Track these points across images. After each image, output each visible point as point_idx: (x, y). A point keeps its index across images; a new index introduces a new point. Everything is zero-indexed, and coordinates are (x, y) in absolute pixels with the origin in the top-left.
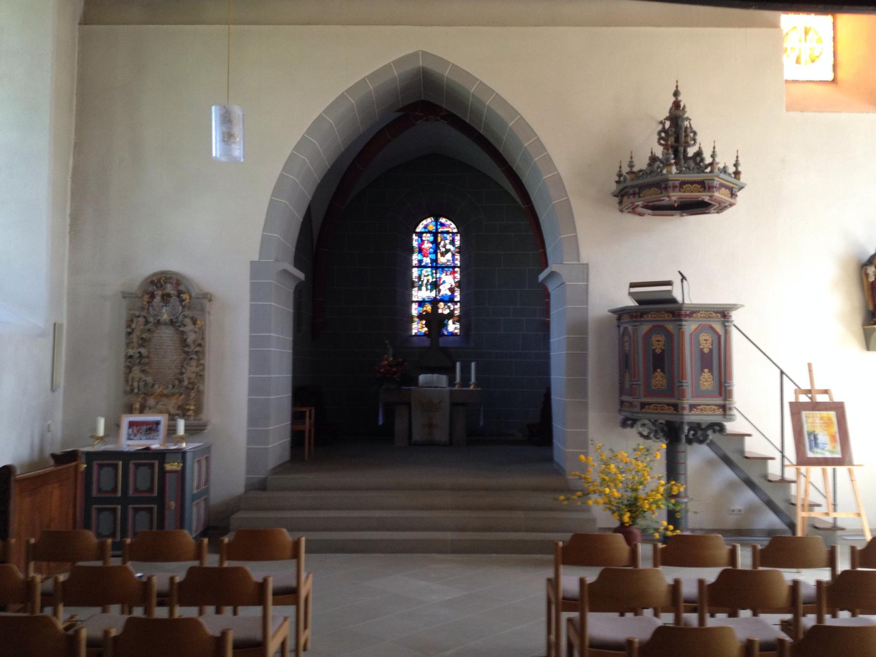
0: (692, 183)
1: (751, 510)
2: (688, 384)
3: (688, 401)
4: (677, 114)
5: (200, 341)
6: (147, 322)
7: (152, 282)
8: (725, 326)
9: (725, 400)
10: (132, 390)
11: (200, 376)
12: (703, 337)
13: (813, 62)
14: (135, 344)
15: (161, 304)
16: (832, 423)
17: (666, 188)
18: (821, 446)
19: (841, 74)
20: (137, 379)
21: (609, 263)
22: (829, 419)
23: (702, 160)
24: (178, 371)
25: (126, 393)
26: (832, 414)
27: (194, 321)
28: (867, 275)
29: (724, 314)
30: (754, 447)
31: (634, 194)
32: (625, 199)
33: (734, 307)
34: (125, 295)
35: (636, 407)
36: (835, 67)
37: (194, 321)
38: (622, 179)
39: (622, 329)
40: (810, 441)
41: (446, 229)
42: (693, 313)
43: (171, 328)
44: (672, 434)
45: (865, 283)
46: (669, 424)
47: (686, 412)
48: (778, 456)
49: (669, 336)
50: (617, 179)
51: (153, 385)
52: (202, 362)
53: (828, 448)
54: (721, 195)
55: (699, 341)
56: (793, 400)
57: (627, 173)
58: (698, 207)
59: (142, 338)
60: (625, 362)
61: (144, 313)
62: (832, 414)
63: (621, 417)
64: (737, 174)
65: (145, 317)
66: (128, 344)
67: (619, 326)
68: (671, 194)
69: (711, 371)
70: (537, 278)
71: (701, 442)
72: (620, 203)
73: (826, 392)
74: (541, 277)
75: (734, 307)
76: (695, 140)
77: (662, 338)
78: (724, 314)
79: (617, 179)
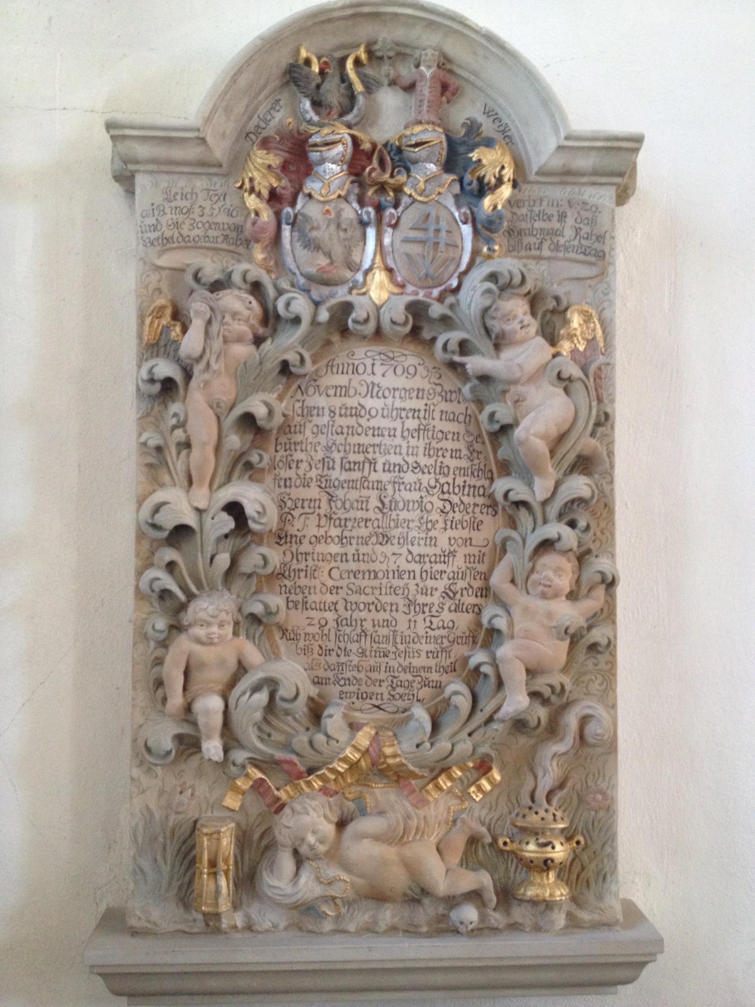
5: (588, 444)
6: (271, 320)
7: (294, 76)
10: (189, 744)
11: (590, 648)
14: (202, 456)
15: (350, 211)
20: (220, 676)
24: (464, 621)
25: (145, 753)
27: (550, 318)
34: (136, 155)
37: (550, 318)
41: (363, 566)
43: (410, 358)
51: (316, 712)
52: (602, 564)
59: (248, 420)
61: (254, 263)
65: (256, 288)
66: (155, 461)
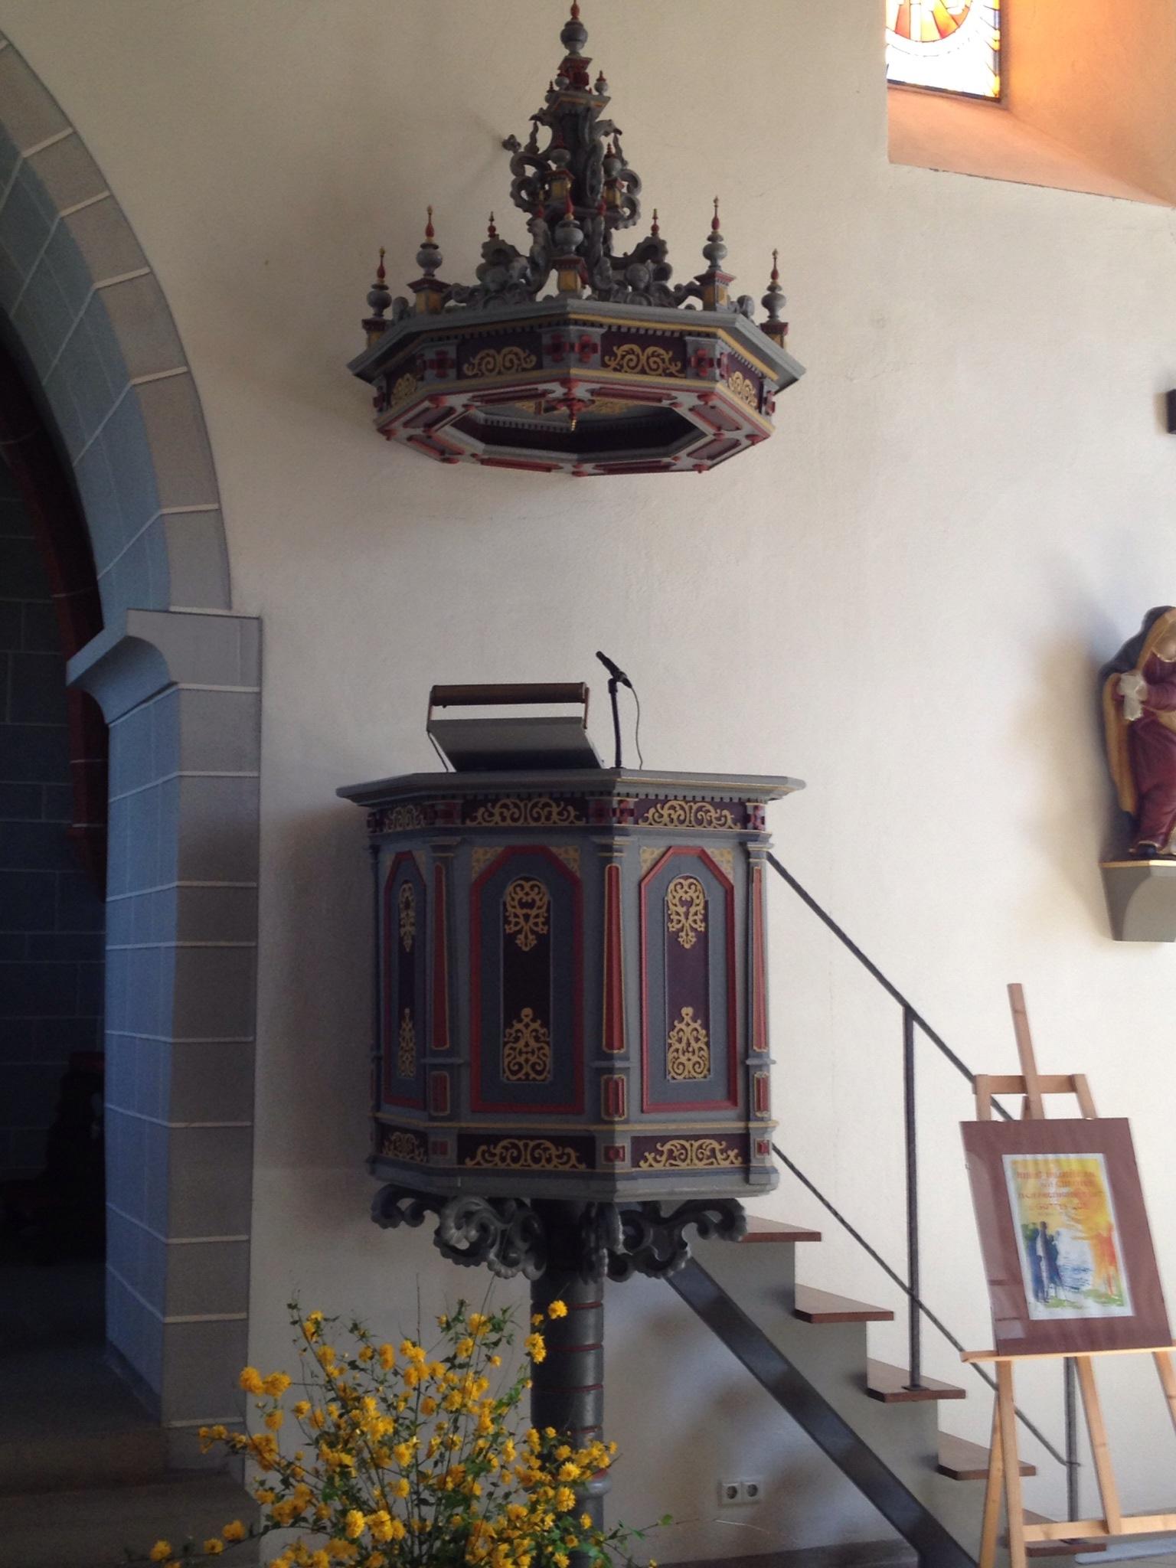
0: (644, 339)
1: (791, 1482)
2: (629, 1062)
3: (626, 1130)
4: (573, 106)
8: (747, 854)
9: (747, 1118)
12: (679, 891)
13: (943, 34)
16: (1098, 1193)
17: (558, 350)
18: (1067, 1277)
19: (1023, 81)
21: (342, 621)
22: (1089, 1180)
23: (664, 272)
26: (1095, 1162)
28: (1120, 702)
29: (741, 808)
30: (825, 1273)
31: (440, 364)
32: (403, 385)
33: (776, 787)
35: (443, 1149)
36: (1002, 59)
38: (388, 314)
39: (387, 860)
40: (1035, 1260)
42: (647, 803)
44: (565, 1243)
45: (1113, 732)
46: (550, 1211)
47: (623, 1166)
48: (900, 1303)
49: (565, 885)
50: (369, 313)
53: (1095, 1292)
54: (732, 393)
55: (665, 904)
56: (972, 1117)
57: (416, 286)
58: (647, 440)
60: (400, 982)
62: (1095, 1162)
63: (375, 1186)
64: (775, 329)
67: (375, 850)
68: (574, 372)
69: (703, 1014)
70: (63, 672)
71: (654, 1268)
72: (382, 401)
73: (1071, 1084)
74: (79, 665)
75: (776, 787)
76: (633, 205)
77: (542, 896)
78: (741, 808)
79: (369, 313)
